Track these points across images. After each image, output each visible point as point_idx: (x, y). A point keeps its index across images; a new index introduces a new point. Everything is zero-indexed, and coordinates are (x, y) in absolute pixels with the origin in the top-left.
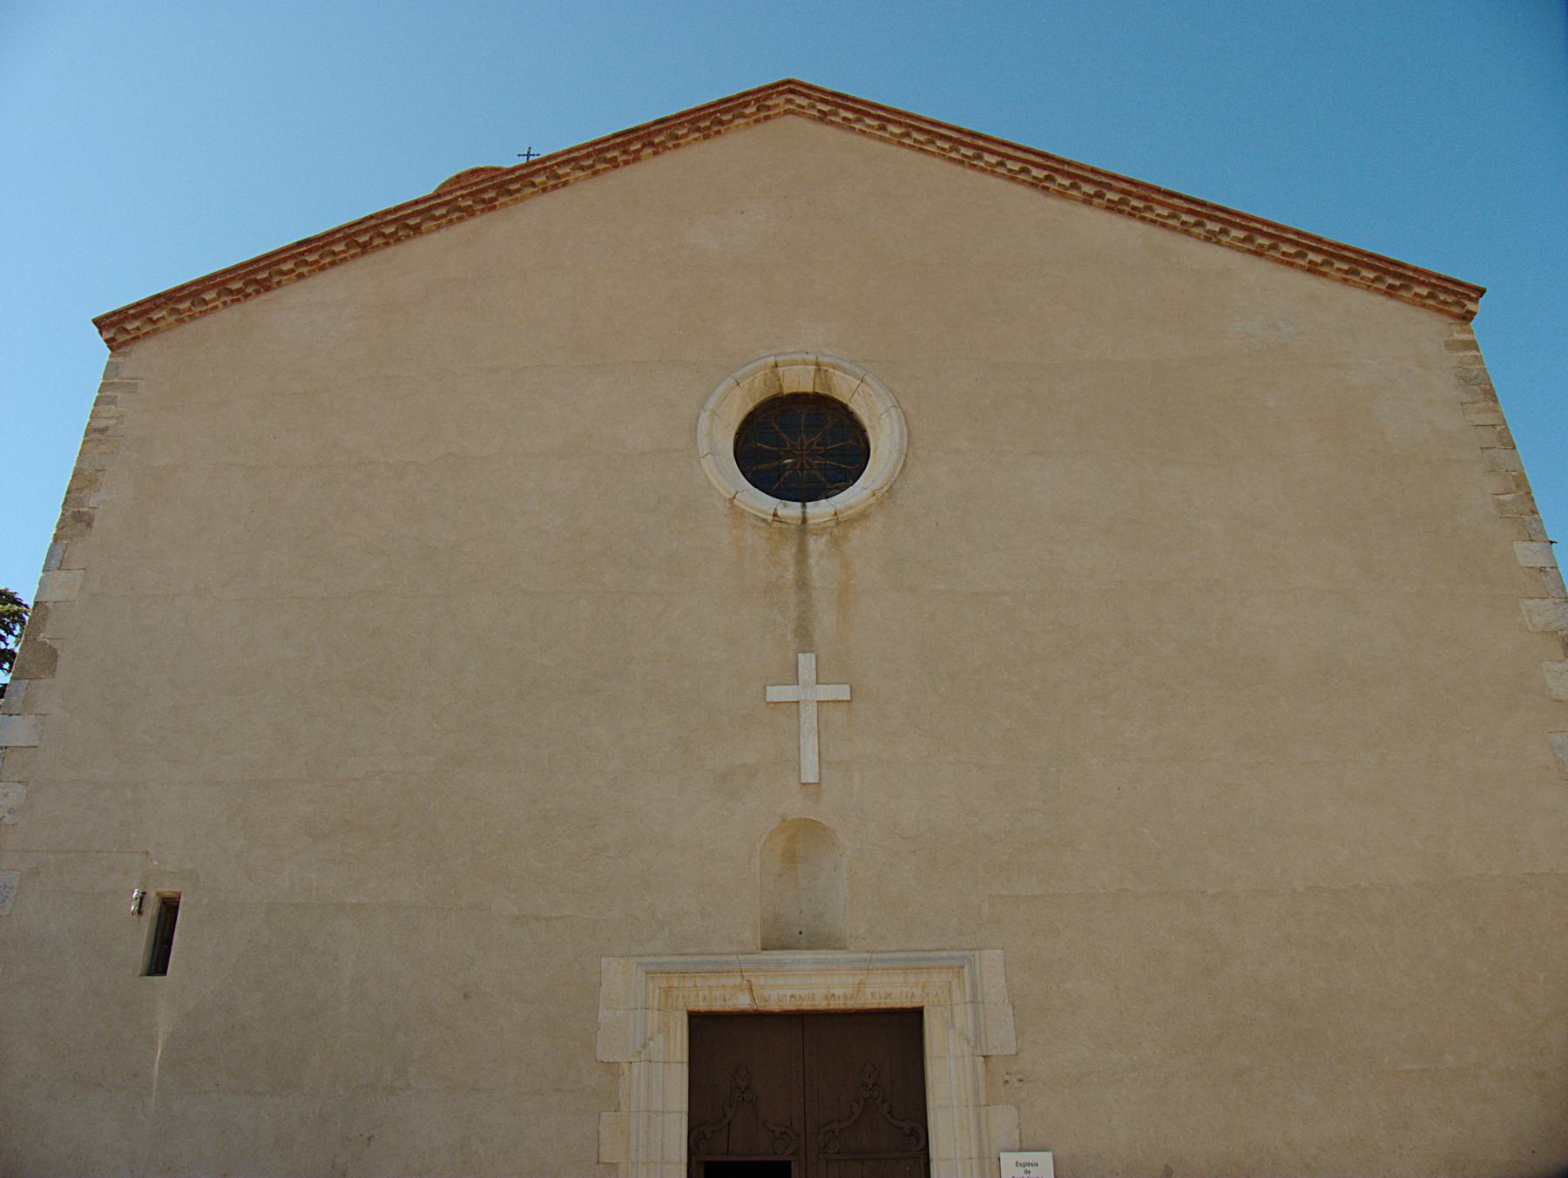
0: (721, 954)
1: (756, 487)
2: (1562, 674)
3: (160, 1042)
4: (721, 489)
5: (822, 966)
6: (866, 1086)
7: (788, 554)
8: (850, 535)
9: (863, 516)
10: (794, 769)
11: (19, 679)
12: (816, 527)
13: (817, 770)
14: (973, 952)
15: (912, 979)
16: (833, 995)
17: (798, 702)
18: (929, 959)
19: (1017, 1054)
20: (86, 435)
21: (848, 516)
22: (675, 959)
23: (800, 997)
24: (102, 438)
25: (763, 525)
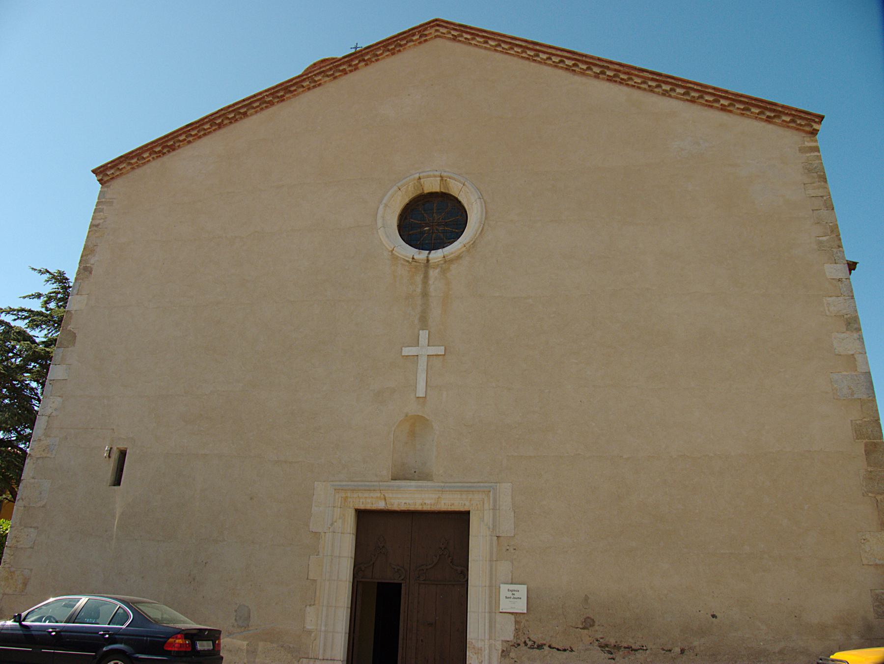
4: (387, 246)
5: (420, 489)
6: (441, 549)
7: (419, 278)
9: (459, 257)
14: (496, 484)
16: (425, 503)
17: (417, 356)
18: (473, 487)
20: (90, 228)
22: (349, 483)
23: (409, 503)
25: (407, 264)
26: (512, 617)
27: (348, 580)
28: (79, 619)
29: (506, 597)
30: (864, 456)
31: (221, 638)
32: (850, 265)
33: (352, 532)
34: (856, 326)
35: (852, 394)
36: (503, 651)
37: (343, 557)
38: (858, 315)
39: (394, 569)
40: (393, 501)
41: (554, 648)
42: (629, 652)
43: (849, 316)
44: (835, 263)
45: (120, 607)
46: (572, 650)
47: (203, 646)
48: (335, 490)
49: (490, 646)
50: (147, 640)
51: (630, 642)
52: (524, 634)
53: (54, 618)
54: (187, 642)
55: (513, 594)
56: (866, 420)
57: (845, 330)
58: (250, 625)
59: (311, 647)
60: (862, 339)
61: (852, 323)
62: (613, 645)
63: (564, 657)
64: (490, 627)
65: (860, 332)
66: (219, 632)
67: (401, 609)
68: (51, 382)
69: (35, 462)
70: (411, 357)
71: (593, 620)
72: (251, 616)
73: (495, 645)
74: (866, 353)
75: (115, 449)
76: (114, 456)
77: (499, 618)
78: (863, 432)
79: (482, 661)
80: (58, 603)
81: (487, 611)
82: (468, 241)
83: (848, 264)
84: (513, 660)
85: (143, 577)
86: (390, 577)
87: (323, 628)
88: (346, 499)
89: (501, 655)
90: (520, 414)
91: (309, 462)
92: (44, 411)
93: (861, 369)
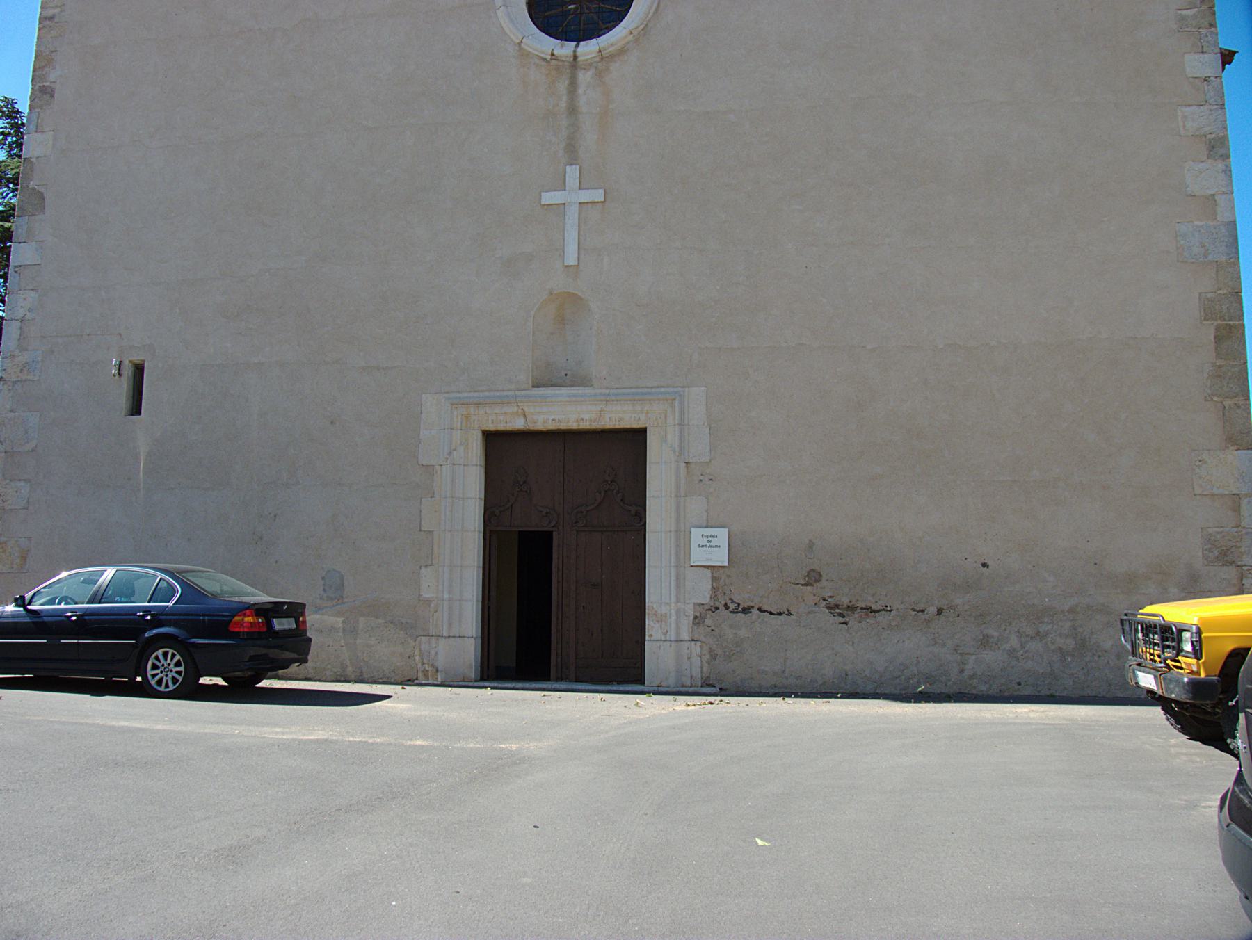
0: (503, 391)
1: (542, 31)
2: (1201, 172)
3: (142, 458)
4: (512, 36)
5: (574, 399)
6: (607, 482)
7: (562, 86)
8: (611, 68)
9: (622, 51)
10: (560, 255)
11: (22, 216)
12: (584, 62)
13: (577, 255)
14: (683, 389)
15: (638, 408)
16: (582, 419)
17: (564, 204)
18: (650, 393)
19: (710, 461)
20: (40, 23)
21: (610, 52)
22: (471, 394)
23: (559, 420)
24: (52, 24)
25: (544, 63)
26: (708, 573)
27: (477, 530)
28: (105, 598)
29: (699, 545)
30: (1213, 346)
31: (306, 614)
32: (1225, 55)
33: (478, 464)
34: (1222, 151)
35: (1206, 256)
36: (696, 618)
37: (468, 498)
38: (1227, 135)
39: (541, 512)
40: (535, 417)
41: (765, 611)
42: (867, 615)
43: (1213, 136)
44: (1202, 52)
45: (161, 579)
46: (789, 614)
47: (280, 624)
48: (452, 404)
49: (678, 612)
50: (204, 620)
51: (868, 600)
52: (725, 594)
53: (71, 599)
54: (260, 620)
55: (709, 541)
56: (1221, 292)
57: (1205, 157)
58: (344, 596)
59: (431, 621)
60: (1230, 171)
61: (1217, 147)
62: (845, 606)
63: (779, 622)
64: (678, 586)
65: (1228, 160)
66: (303, 606)
67: (553, 566)
68: (17, 269)
69: (10, 388)
70: (555, 207)
71: (820, 573)
72: (346, 583)
73: (684, 609)
74: (1232, 193)
75: (126, 362)
76: (126, 373)
77: (689, 573)
78: (1215, 310)
79: (667, 631)
80: (74, 579)
81: (673, 564)
82: (636, 25)
83: (1222, 53)
84: (709, 629)
85: (189, 540)
86: (535, 523)
87: (446, 596)
88: (468, 417)
89: (693, 623)
90: (718, 288)
91: (412, 366)
92: (13, 314)
93: (1223, 216)
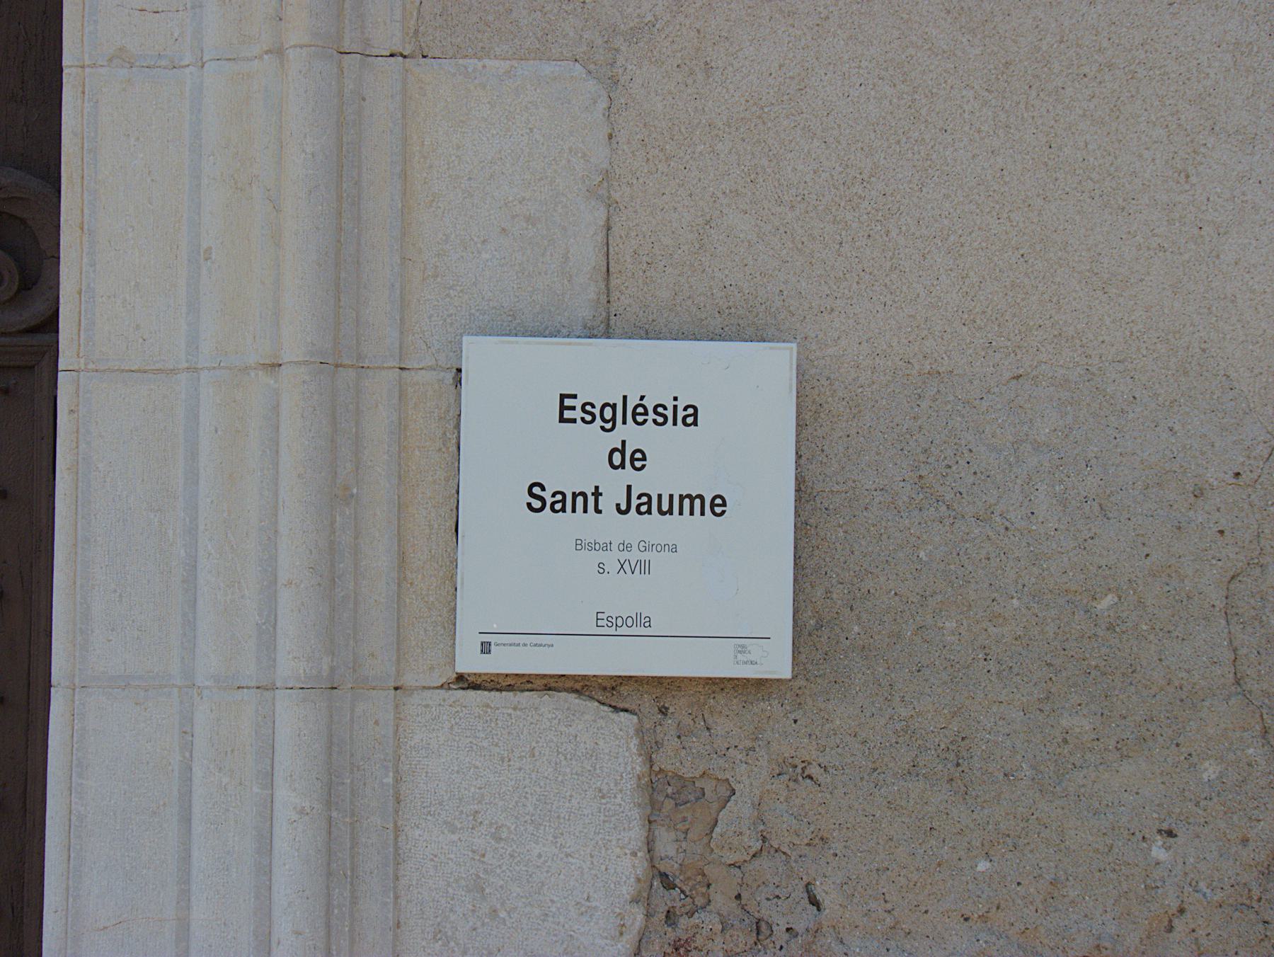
81: (289, 665)
